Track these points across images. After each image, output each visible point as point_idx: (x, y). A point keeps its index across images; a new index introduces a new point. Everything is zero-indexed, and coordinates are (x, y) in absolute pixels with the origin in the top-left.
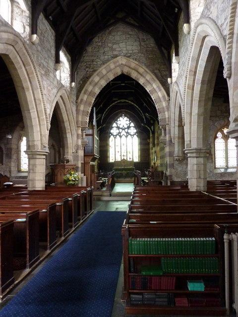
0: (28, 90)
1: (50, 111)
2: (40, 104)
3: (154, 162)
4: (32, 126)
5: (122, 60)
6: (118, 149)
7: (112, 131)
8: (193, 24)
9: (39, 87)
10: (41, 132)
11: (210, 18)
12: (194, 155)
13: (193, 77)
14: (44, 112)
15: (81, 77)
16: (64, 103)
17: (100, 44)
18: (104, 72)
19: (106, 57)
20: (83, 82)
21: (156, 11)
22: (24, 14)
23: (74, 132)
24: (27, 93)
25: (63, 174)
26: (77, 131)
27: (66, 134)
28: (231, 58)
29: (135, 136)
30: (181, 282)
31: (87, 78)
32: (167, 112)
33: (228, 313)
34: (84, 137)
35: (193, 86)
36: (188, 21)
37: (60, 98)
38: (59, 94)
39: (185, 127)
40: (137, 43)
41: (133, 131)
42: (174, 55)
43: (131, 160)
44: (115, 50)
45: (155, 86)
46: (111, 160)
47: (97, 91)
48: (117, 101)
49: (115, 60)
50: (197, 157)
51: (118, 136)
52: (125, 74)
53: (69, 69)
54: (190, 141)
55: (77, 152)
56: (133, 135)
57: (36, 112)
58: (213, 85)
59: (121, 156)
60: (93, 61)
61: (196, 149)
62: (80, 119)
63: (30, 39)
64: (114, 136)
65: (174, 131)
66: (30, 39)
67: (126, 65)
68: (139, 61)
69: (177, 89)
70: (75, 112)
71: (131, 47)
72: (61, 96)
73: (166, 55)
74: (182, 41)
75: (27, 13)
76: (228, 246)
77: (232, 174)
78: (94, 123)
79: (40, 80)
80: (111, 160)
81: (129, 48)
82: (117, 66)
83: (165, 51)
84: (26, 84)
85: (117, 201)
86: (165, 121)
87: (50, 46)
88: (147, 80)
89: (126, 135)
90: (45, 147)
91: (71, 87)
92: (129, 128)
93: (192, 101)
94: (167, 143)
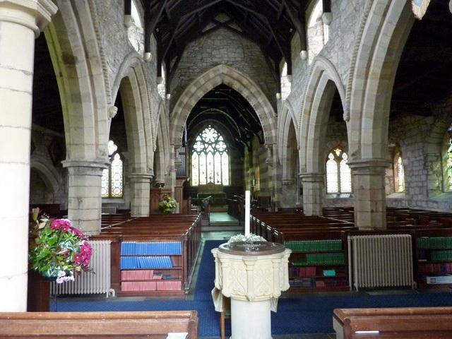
0: (139, 110)
4: (139, 148)
5: (222, 69)
6: (203, 169)
7: (195, 146)
10: (147, 154)
12: (310, 179)
13: (310, 103)
15: (176, 86)
17: (197, 49)
18: (202, 81)
19: (205, 64)
21: (267, 23)
22: (138, 31)
23: (167, 151)
24: (137, 113)
25: (157, 200)
26: (170, 149)
28: (349, 106)
29: (225, 153)
30: (320, 269)
32: (275, 132)
33: (351, 289)
35: (310, 112)
39: (300, 151)
40: (239, 50)
41: (222, 146)
43: (220, 183)
45: (260, 100)
46: (195, 183)
47: (193, 103)
49: (215, 68)
50: (312, 182)
51: (203, 153)
54: (306, 165)
56: (222, 152)
58: (329, 111)
59: (206, 178)
60: (189, 68)
61: (312, 174)
62: (173, 136)
64: (197, 152)
65: (283, 151)
68: (242, 71)
73: (274, 65)
75: (142, 31)
76: (384, 55)
77: (345, 200)
80: (195, 183)
81: (232, 55)
82: (217, 75)
84: (138, 104)
85: (213, 231)
86: (272, 141)
88: (251, 93)
90: (151, 170)
91: (166, 100)
92: (217, 142)
93: (308, 125)
94: (275, 165)
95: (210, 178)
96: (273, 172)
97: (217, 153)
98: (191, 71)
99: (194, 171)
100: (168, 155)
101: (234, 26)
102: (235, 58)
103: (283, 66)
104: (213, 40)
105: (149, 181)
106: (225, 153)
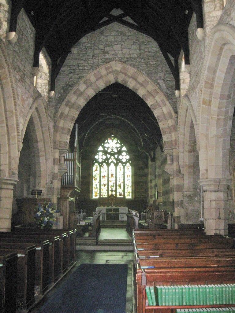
1: (23, 127)
2: (12, 116)
3: (153, 199)
5: (117, 66)
6: (104, 181)
7: (96, 157)
8: (208, 29)
9: (12, 95)
11: (231, 25)
14: (16, 127)
16: (40, 117)
17: (89, 45)
19: (96, 61)
20: (65, 92)
27: (39, 157)
29: (128, 164)
31: (70, 86)
34: (62, 162)
36: (201, 24)
37: (35, 110)
38: (35, 105)
41: (125, 157)
42: (183, 63)
43: (122, 197)
44: (107, 53)
47: (82, 102)
48: (106, 116)
49: (108, 65)
51: (105, 164)
52: (120, 83)
53: (48, 74)
54: (207, 170)
55: (52, 183)
56: (126, 163)
57: (6, 127)
63: (7, 37)
64: (99, 163)
65: (185, 158)
66: (7, 37)
67: (159, 85)
68: (138, 68)
69: (188, 104)
70: (52, 130)
71: (128, 50)
72: (36, 108)
73: (173, 62)
74: (194, 46)
78: (76, 144)
79: (15, 86)
82: (110, 73)
83: (172, 59)
87: (29, 46)
88: (148, 91)
89: (115, 161)
90: (14, 173)
91: (49, 98)
92: (120, 152)
95: (112, 191)
96: (174, 182)
97: (120, 164)
98: (81, 68)
99: (95, 183)
100: (51, 161)
101: (128, 19)
102: (130, 54)
103: (182, 60)
104: (107, 36)
105: (12, 187)
106: (128, 164)
